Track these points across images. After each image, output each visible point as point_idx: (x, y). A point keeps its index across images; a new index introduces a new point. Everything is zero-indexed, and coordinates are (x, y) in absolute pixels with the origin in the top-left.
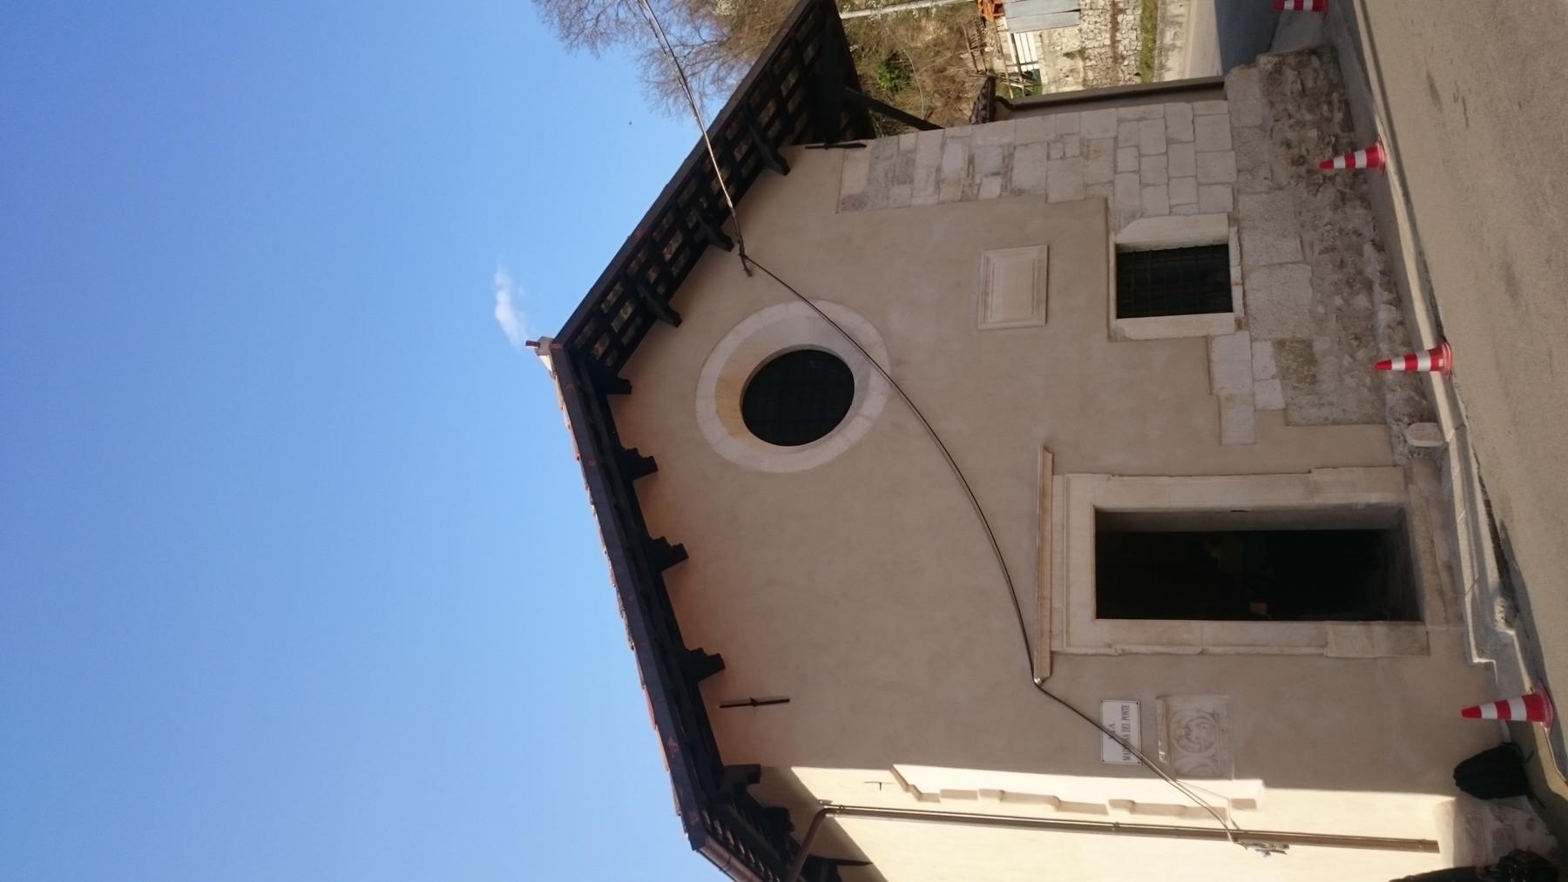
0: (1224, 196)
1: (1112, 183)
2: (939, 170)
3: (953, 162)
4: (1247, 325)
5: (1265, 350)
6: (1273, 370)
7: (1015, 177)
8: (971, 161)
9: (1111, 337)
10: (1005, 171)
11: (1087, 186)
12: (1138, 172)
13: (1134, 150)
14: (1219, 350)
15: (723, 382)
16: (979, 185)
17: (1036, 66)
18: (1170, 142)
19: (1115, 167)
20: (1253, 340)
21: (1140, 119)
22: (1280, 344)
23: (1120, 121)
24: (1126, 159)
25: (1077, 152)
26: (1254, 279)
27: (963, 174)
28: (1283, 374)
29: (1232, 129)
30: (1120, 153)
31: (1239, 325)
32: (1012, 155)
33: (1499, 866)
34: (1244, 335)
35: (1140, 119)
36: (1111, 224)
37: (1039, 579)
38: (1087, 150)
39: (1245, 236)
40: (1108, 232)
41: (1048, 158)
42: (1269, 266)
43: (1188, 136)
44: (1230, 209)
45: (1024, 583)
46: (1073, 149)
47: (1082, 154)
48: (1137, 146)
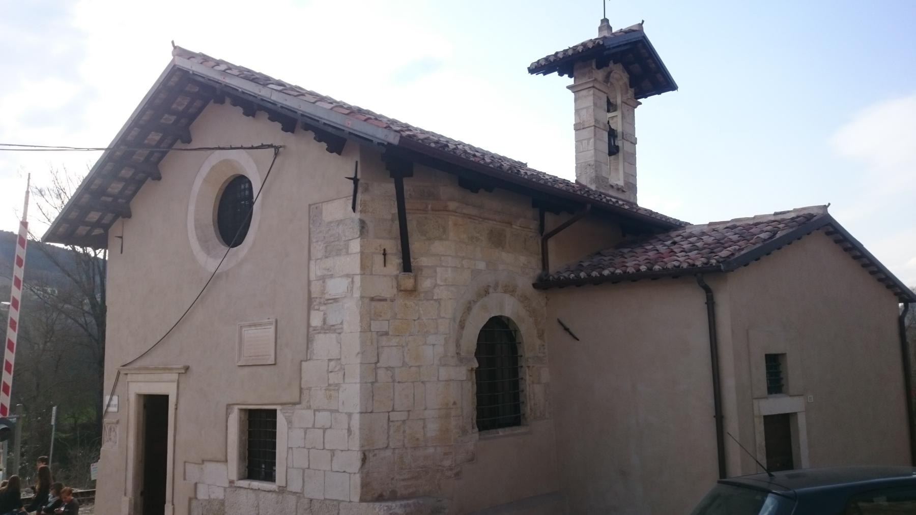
0: (295, 486)
1: (309, 408)
2: (332, 276)
3: (337, 287)
4: (231, 487)
5: (219, 494)
6: (212, 497)
7: (320, 335)
8: (335, 300)
9: (229, 407)
10: (327, 328)
11: (310, 389)
12: (314, 427)
13: (328, 425)
14: (221, 466)
15: (204, 242)
16: (318, 310)
17: (245, 483)
18: (333, 452)
19: (318, 410)
20: (225, 488)
21: (349, 430)
22: (222, 503)
23: (350, 415)
24: (323, 418)
25: (331, 382)
26: (252, 495)
27: (327, 297)
28: (210, 501)
29: (339, 502)
30: (327, 414)
31: (231, 482)
32: (335, 331)
33: (89, 466)
34: (227, 485)
35: (349, 430)
36: (285, 406)
37: (139, 369)
38: (332, 389)
39: (274, 495)
40: (281, 404)
41: (330, 360)
42: (258, 506)
43: (335, 468)
44: (289, 489)
45: (138, 364)
46: (334, 378)
47: (329, 385)
48: (330, 428)
